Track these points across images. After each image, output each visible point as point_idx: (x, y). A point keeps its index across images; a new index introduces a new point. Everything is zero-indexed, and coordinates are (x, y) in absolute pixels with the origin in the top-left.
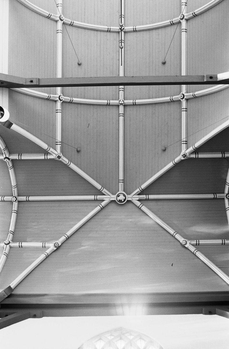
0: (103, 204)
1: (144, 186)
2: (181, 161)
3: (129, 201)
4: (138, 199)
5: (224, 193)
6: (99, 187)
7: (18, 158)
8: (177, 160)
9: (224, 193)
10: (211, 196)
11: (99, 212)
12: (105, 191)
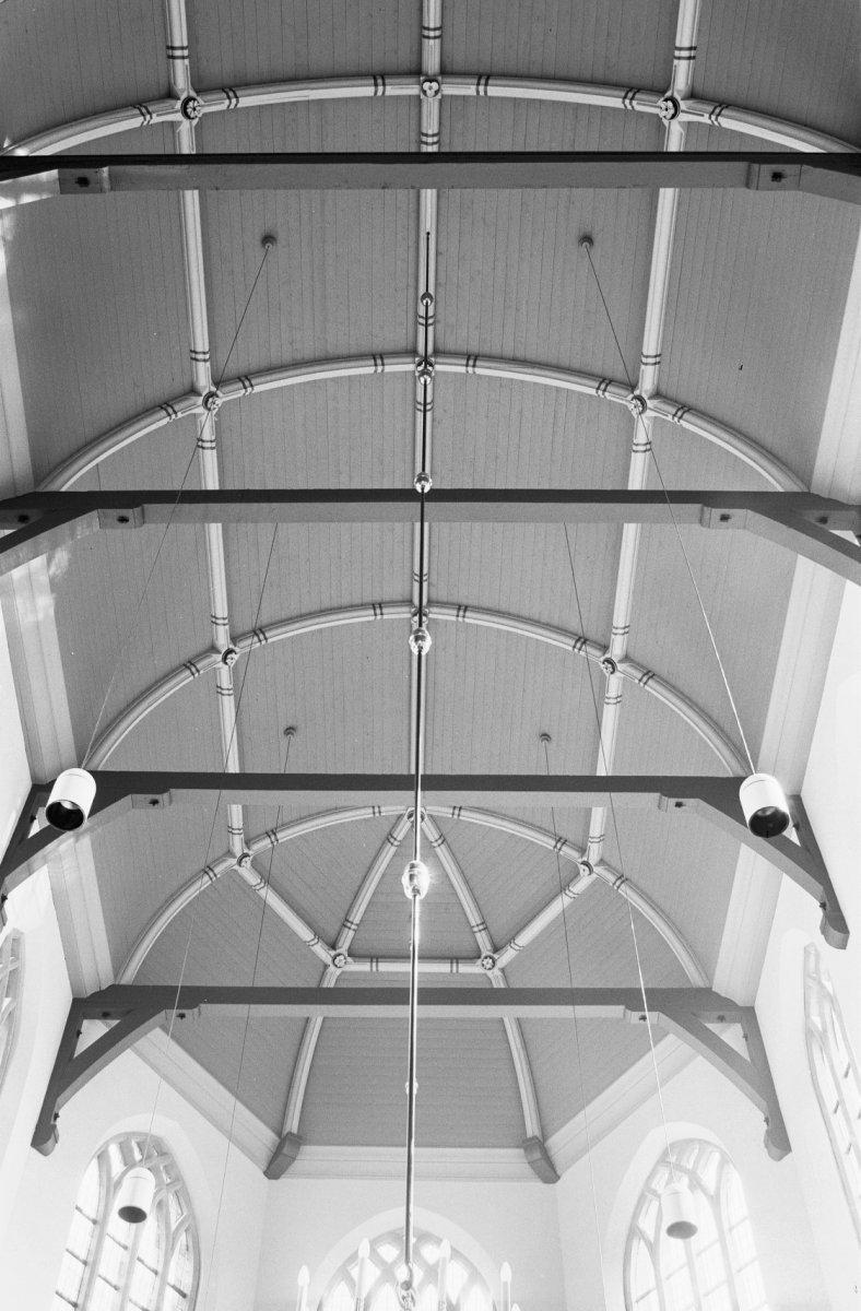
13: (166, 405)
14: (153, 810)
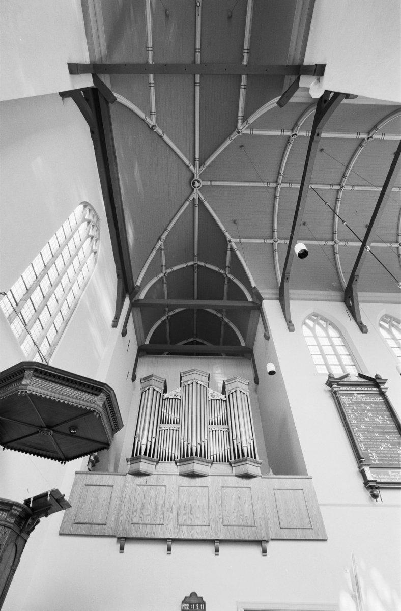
0: (192, 167)
1: (206, 203)
2: (225, 238)
3: (193, 190)
4: (195, 197)
5: (198, 260)
6: (207, 164)
7: (242, 84)
8: (227, 234)
9: (198, 260)
10: (196, 253)
11: (185, 164)
12: (203, 169)
13: (335, 253)
14: (358, 281)
